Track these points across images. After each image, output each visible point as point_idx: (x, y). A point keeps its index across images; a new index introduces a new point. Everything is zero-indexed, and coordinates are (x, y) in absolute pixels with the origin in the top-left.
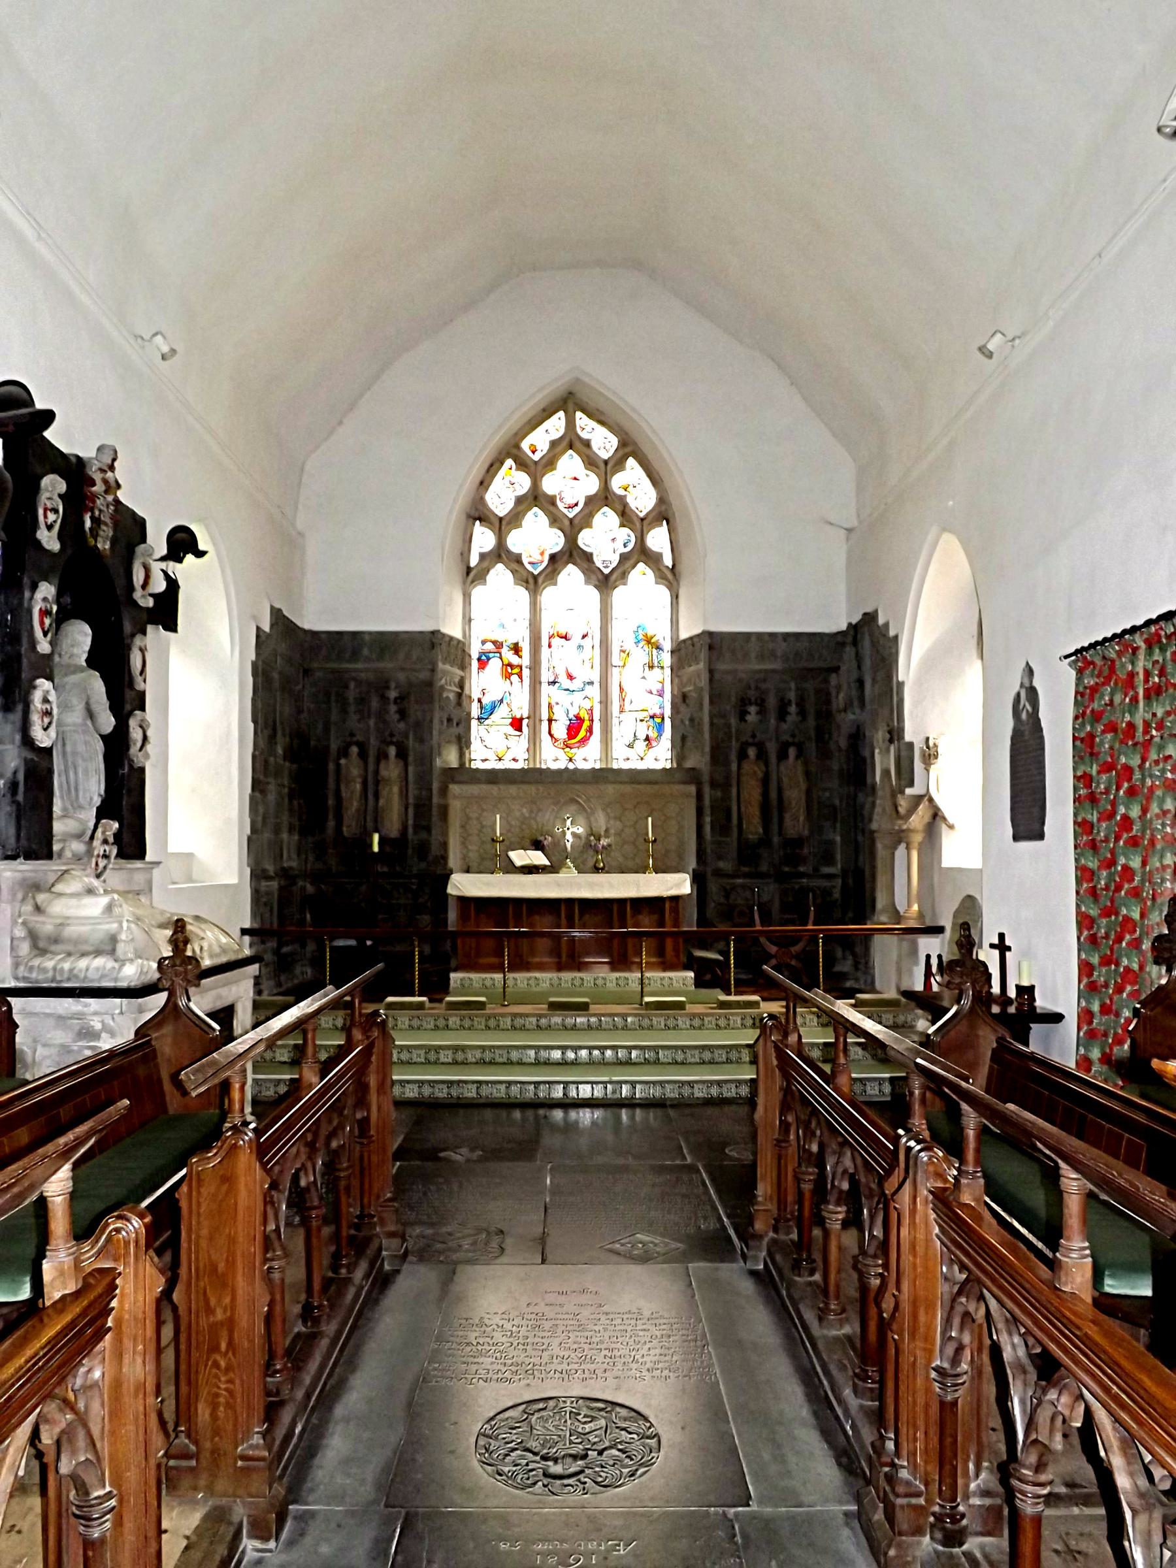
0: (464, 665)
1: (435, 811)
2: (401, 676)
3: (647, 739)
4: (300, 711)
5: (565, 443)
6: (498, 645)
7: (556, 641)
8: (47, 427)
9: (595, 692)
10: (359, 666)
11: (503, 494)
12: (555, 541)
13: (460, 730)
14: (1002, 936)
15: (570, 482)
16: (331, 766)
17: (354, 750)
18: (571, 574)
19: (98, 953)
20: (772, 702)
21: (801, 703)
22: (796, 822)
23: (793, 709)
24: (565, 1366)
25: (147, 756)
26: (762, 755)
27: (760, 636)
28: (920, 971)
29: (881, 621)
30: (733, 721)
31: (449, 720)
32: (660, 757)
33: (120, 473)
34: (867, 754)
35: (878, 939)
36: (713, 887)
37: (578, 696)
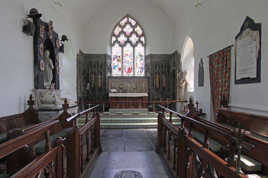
0: (111, 60)
1: (106, 83)
2: (101, 61)
3: (141, 72)
4: (84, 67)
5: (127, 23)
6: (116, 56)
7: (126, 56)
8: (40, 17)
9: (132, 64)
10: (94, 60)
11: (117, 30)
12: (126, 39)
13: (110, 70)
14: (197, 102)
15: (128, 29)
16: (90, 76)
17: (93, 73)
18: (128, 45)
19: (52, 104)
20: (161, 66)
21: (165, 66)
22: (164, 85)
23: (164, 67)
24: (127, 166)
25: (59, 73)
26: (159, 74)
27: (159, 55)
28: (184, 108)
29: (178, 52)
30: (155, 69)
31: (109, 68)
32: (143, 74)
33: (53, 25)
34: (175, 74)
35: (177, 103)
36: (151, 95)
37: (129, 65)
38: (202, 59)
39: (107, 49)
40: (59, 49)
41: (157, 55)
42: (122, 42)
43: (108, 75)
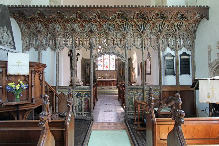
0: (97, 61)
6: (100, 60)
7: (105, 59)
9: (108, 63)
26: (122, 69)
30: (120, 66)
32: (114, 69)
43: (96, 69)
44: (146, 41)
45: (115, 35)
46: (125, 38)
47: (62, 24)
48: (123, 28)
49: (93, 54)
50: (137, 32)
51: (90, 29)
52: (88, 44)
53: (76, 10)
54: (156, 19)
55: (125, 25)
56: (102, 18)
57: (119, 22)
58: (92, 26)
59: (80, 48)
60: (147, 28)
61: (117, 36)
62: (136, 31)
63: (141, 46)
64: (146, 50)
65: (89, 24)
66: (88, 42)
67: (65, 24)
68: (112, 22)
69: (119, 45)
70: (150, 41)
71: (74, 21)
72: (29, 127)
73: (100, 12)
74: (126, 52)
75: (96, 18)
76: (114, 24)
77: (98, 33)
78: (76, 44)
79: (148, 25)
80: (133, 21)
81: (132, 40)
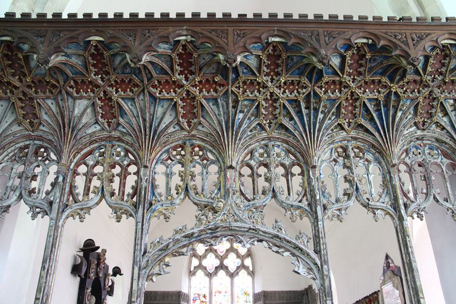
6: (199, 295)
7: (217, 294)
18: (222, 273)
27: (279, 292)
38: (387, 257)
39: (183, 282)
40: (108, 291)
41: (275, 292)
42: (211, 269)
44: (405, 177)
45: (262, 151)
46: (306, 163)
47: (20, 99)
48: (296, 118)
49: (147, 239)
50: (361, 134)
51: (144, 120)
52: (131, 191)
53: (82, 30)
54: (440, 78)
55: (303, 105)
56: (200, 70)
57: (277, 91)
58: (152, 108)
59: (90, 208)
60: (405, 116)
61: (268, 156)
62: (353, 134)
63: (387, 199)
64: (415, 216)
65: (141, 97)
66: (131, 180)
67: (31, 99)
68: (244, 91)
69: (283, 197)
70: (426, 179)
71: (72, 83)
72: (334, 278)
73: (189, 38)
74: (320, 226)
75: (172, 69)
76: (253, 101)
77: (180, 142)
78: (72, 187)
79: (406, 104)
80: (341, 83)
81: (342, 172)
